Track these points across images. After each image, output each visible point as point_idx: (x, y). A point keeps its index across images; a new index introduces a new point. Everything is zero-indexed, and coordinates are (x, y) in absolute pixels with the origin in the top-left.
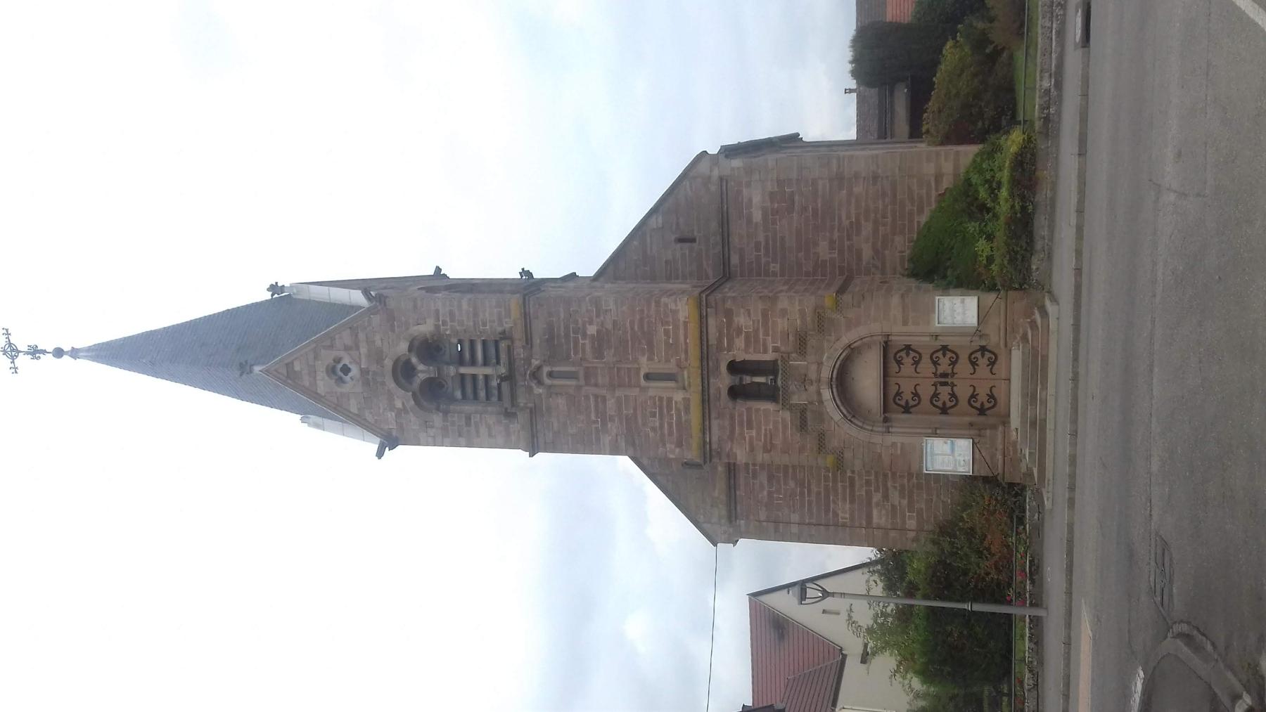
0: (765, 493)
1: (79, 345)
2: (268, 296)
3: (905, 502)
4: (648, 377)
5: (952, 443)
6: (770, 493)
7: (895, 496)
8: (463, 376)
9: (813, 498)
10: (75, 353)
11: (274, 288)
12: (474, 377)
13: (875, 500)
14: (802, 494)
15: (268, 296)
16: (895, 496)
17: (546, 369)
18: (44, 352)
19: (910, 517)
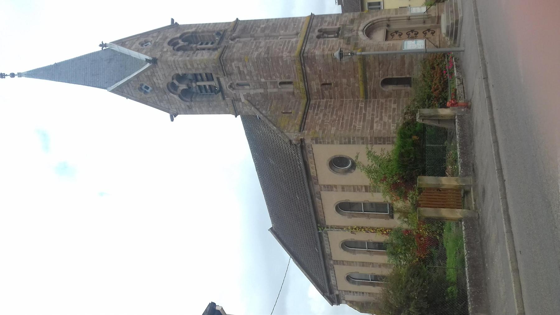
0: (320, 121)
1: (22, 71)
2: (100, 49)
3: (391, 121)
4: (281, 83)
5: (336, 262)
6: (323, 121)
7: (386, 119)
8: (199, 86)
9: (344, 121)
10: (20, 75)
11: (102, 45)
12: (205, 86)
13: (375, 120)
14: (339, 120)
15: (100, 49)
16: (386, 119)
17: (322, 154)
18: (7, 75)
19: (393, 126)
